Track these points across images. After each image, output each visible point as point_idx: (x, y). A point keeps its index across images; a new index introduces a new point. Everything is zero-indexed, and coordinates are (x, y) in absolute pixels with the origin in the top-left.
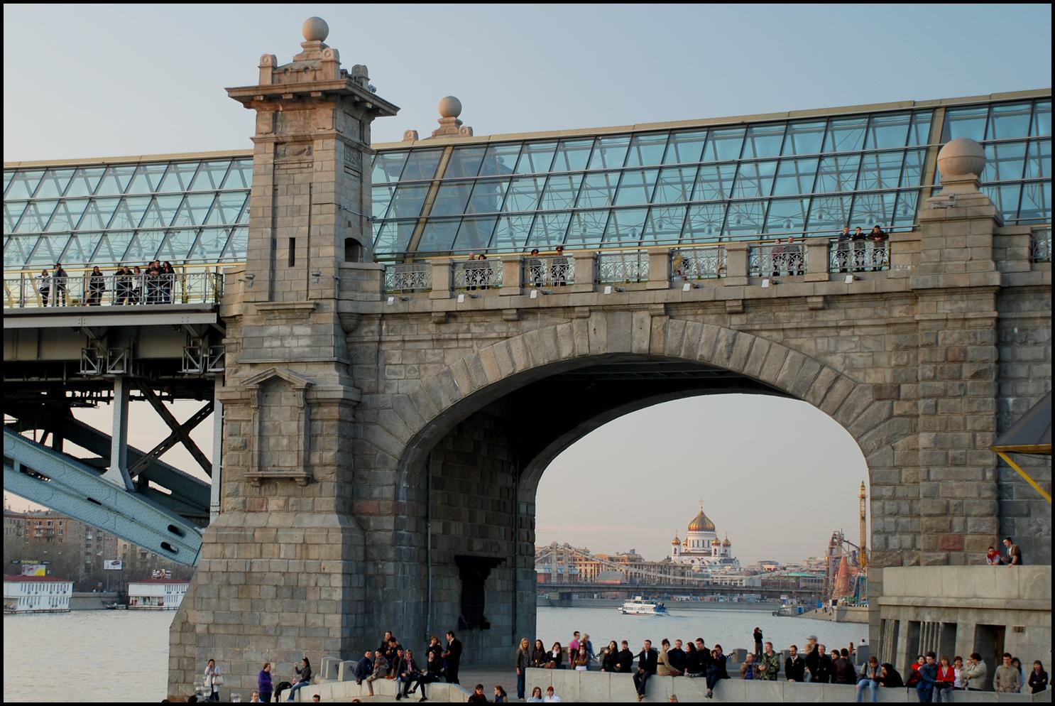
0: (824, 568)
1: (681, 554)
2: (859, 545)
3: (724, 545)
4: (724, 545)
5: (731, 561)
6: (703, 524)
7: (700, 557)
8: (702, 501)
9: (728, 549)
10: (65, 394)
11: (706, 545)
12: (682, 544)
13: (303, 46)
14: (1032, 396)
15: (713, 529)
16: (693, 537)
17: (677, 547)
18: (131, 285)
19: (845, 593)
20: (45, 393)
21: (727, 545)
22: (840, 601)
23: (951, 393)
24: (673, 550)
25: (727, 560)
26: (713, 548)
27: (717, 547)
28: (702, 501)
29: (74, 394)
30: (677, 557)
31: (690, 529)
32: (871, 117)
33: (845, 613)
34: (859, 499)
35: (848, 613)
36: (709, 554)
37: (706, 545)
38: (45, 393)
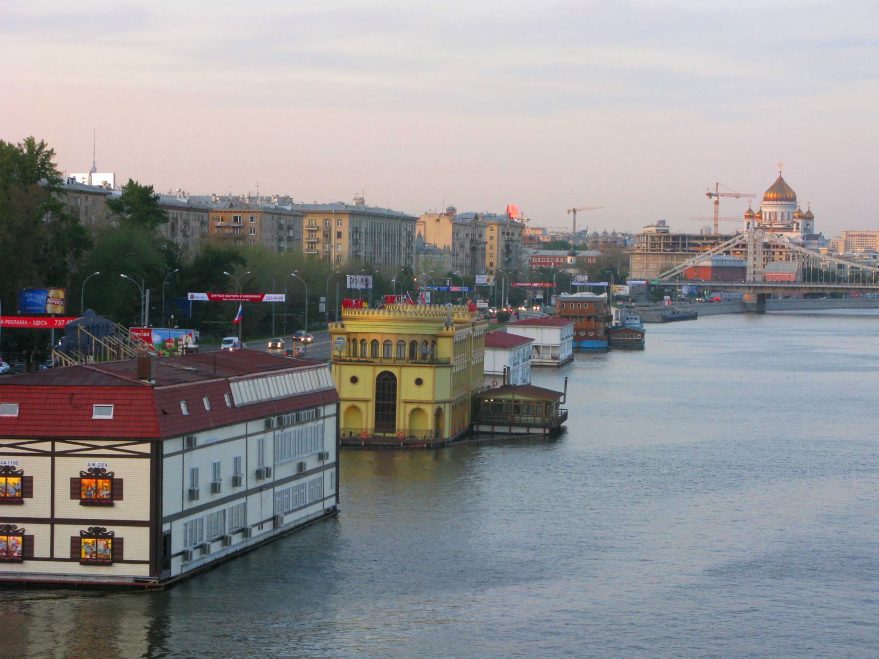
5: (817, 237)
6: (781, 192)
7: (779, 233)
8: (781, 165)
9: (810, 222)
10: (204, 396)
11: (786, 217)
13: (605, 232)
15: (794, 199)
16: (768, 209)
17: (750, 220)
18: (609, 318)
20: (184, 411)
21: (809, 217)
23: (309, 467)
25: (810, 237)
28: (781, 165)
29: (489, 400)
31: (766, 199)
37: (786, 217)
38: (184, 411)
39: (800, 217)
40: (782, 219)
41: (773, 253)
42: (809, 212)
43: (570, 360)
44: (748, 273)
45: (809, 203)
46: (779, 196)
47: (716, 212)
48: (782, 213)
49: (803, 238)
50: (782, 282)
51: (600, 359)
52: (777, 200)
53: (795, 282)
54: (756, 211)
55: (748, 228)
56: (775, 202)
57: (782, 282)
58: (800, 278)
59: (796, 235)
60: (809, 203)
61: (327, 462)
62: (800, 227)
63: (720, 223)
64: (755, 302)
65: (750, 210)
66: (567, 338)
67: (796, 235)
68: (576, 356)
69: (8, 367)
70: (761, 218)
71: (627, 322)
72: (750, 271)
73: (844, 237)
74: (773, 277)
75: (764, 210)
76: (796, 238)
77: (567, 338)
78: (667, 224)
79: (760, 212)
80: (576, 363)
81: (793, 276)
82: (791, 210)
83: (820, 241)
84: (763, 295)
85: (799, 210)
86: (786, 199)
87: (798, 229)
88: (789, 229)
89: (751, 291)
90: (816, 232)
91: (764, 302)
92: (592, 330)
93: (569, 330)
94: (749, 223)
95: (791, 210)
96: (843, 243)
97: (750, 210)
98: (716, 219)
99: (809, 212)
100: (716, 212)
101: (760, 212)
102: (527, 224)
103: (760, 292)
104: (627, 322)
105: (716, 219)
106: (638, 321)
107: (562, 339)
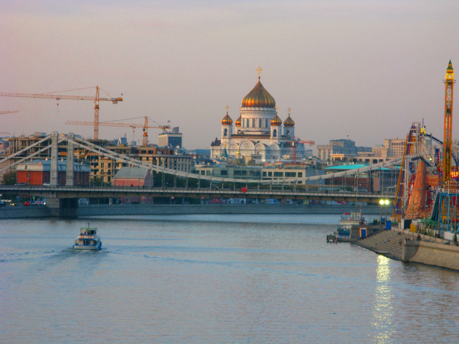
0: (400, 162)
1: (233, 136)
2: (442, 139)
3: (286, 125)
4: (286, 125)
6: (260, 98)
7: (256, 140)
8: (260, 70)
9: (290, 129)
11: (264, 124)
12: (234, 124)
14: (230, 158)
15: (272, 105)
16: (248, 116)
17: (227, 127)
19: (422, 209)
21: (290, 124)
22: (414, 223)
24: (223, 130)
25: (288, 143)
26: (272, 128)
27: (277, 128)
28: (260, 70)
30: (227, 140)
31: (244, 105)
32: (452, 95)
33: (416, 250)
34: (444, 86)
35: (420, 249)
36: (266, 135)
40: (260, 126)
41: (141, 158)
42: (289, 119)
44: (51, 177)
45: (289, 109)
46: (257, 101)
47: (97, 116)
48: (260, 120)
49: (280, 146)
50: (123, 187)
52: (255, 106)
53: (144, 187)
55: (225, 134)
56: (253, 109)
57: (123, 187)
58: (151, 182)
60: (289, 109)
63: (101, 128)
64: (58, 207)
65: (227, 117)
73: (387, 144)
74: (123, 182)
75: (243, 116)
76: (273, 145)
78: (180, 131)
79: (240, 119)
81: (143, 181)
86: (263, 106)
87: (275, 135)
89: (55, 196)
94: (226, 130)
96: (386, 151)
97: (227, 117)
98: (97, 124)
99: (289, 119)
100: (97, 116)
101: (240, 119)
102: (299, 142)
103: (63, 196)
105: (97, 124)
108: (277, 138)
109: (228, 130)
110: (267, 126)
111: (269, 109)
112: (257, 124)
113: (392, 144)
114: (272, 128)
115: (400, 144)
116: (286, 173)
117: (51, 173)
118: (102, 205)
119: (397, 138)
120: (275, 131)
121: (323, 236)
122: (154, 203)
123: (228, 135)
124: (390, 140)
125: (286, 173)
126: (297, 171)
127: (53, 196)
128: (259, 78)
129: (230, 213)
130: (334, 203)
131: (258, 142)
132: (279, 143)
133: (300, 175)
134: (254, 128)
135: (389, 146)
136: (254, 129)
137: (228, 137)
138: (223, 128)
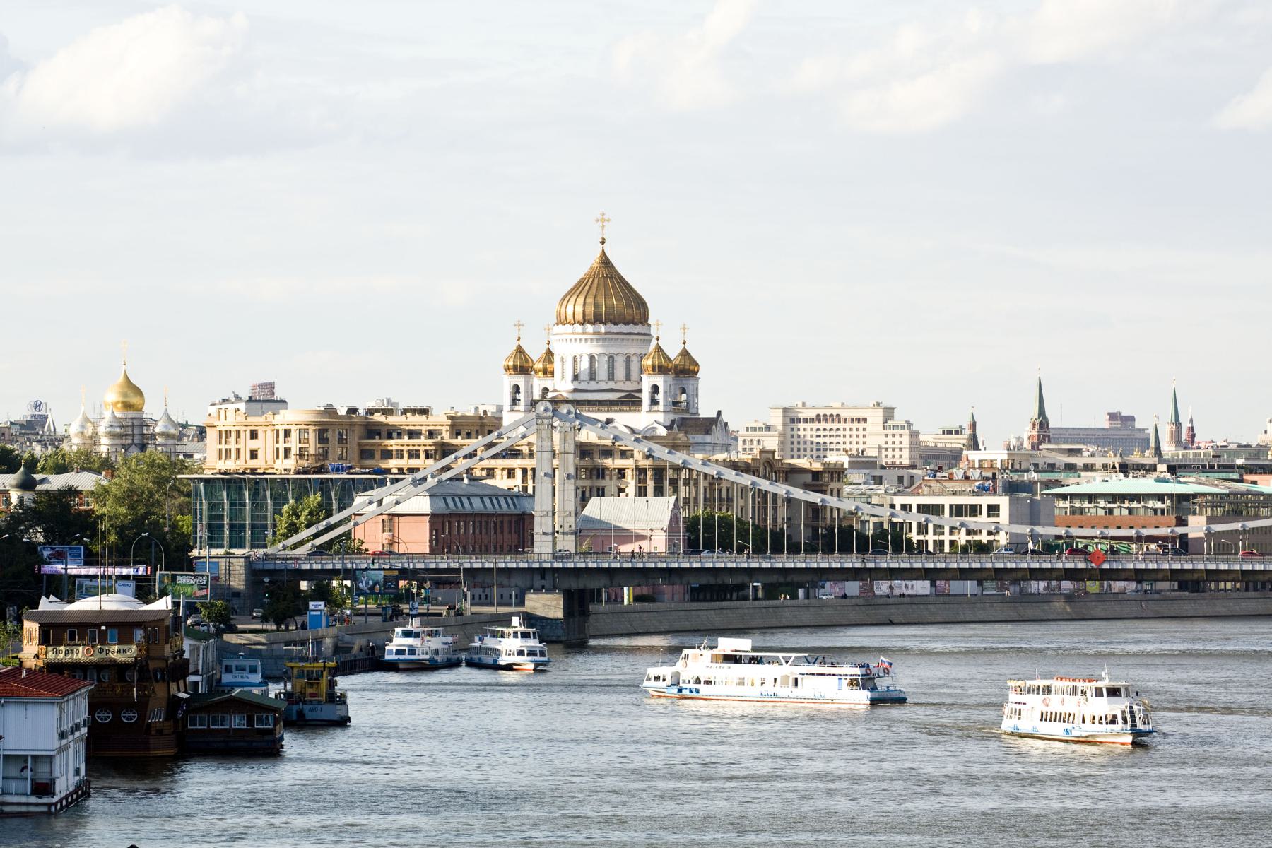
5: (709, 425)
9: (541, 374)
11: (620, 372)
17: (520, 380)
21: (684, 370)
31: (561, 321)
39: (660, 369)
40: (611, 376)
42: (685, 354)
43: (81, 793)
44: (538, 530)
49: (669, 428)
51: (157, 791)
54: (535, 353)
55: (514, 401)
59: (649, 419)
61: (1015, 706)
62: (660, 397)
66: (72, 731)
67: (649, 419)
68: (96, 784)
69: (559, 614)
70: (548, 373)
71: (227, 678)
72: (541, 526)
73: (777, 420)
77: (72, 731)
79: (549, 355)
80: (94, 803)
82: (632, 349)
83: (716, 437)
84: (582, 592)
85: (659, 349)
87: (654, 402)
88: (631, 401)
90: (706, 410)
91: (585, 613)
92: (131, 706)
93: (78, 709)
94: (517, 389)
95: (632, 349)
97: (520, 350)
99: (685, 354)
104: (227, 678)
106: (257, 678)
107: (62, 735)
108: (661, 407)
109: (661, 390)
110: (628, 377)
111: (631, 328)
112: (602, 373)
113: (792, 420)
114: (648, 381)
115: (812, 420)
116: (951, 506)
117: (537, 520)
118: (695, 605)
119: (804, 404)
120: (655, 389)
121: (845, 682)
122: (692, 600)
123: (661, 403)
124: (785, 410)
125: (951, 506)
126: (985, 501)
127: (543, 582)
128: (603, 243)
129: (891, 623)
130: (970, 587)
131: (609, 421)
132: (668, 424)
133: (994, 509)
134: (593, 383)
135: (784, 425)
136: (593, 386)
137: (661, 407)
138: (509, 381)
